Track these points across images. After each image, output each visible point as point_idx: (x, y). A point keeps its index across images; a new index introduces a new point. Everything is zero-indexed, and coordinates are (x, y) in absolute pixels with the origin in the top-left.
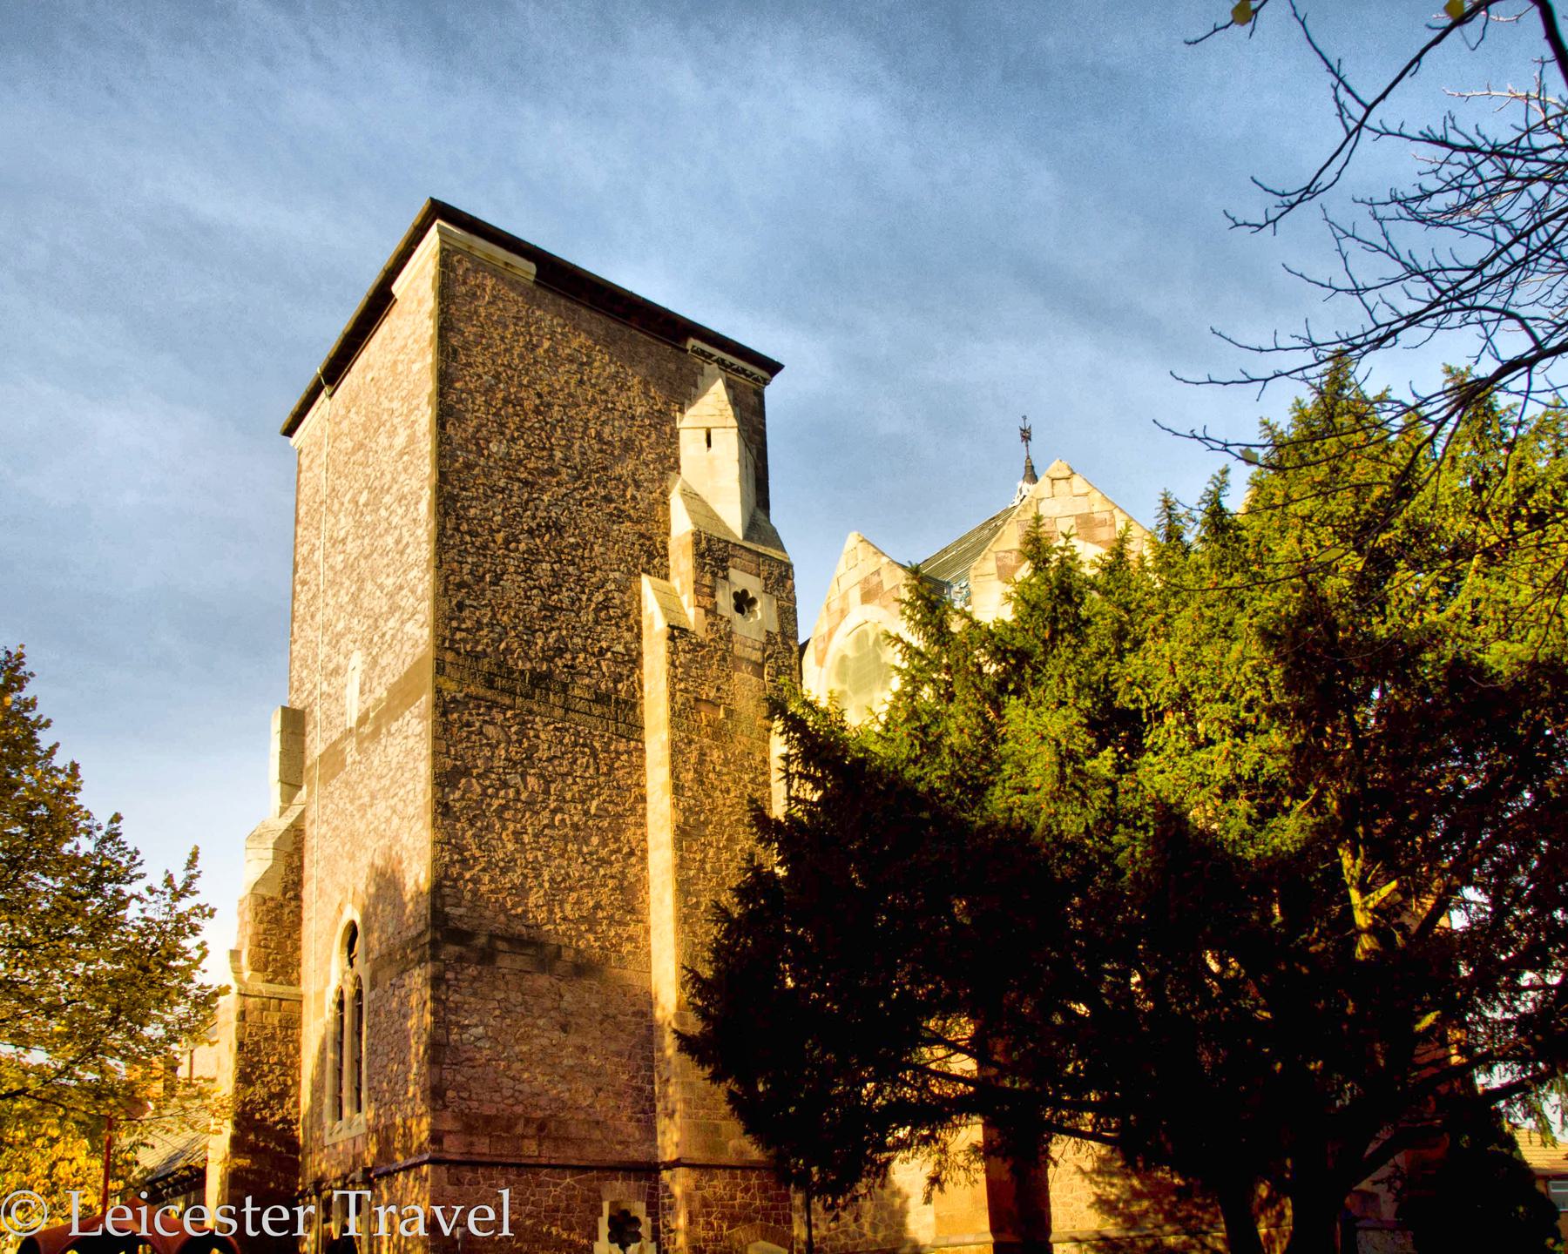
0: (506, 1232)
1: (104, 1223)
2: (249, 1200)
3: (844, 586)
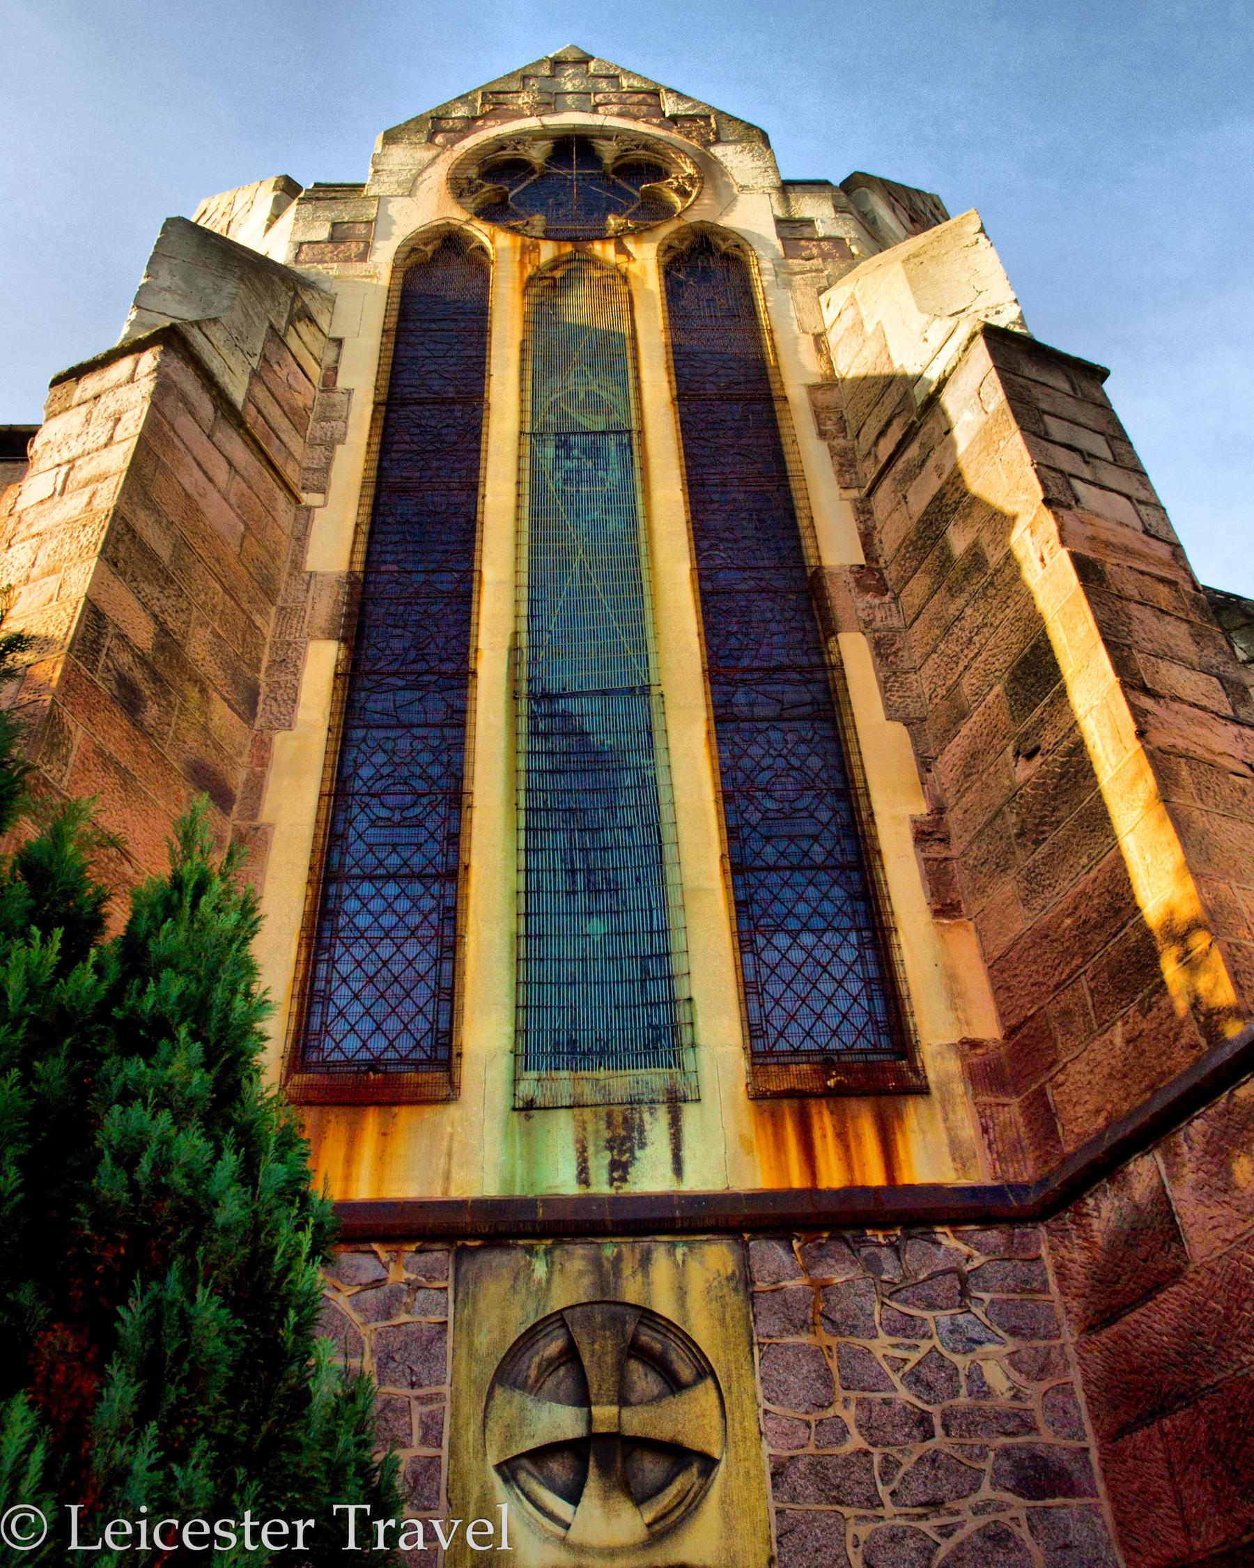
0: (300, 1545)
1: (103, 1536)
2: (248, 1514)
3: (52, 583)
